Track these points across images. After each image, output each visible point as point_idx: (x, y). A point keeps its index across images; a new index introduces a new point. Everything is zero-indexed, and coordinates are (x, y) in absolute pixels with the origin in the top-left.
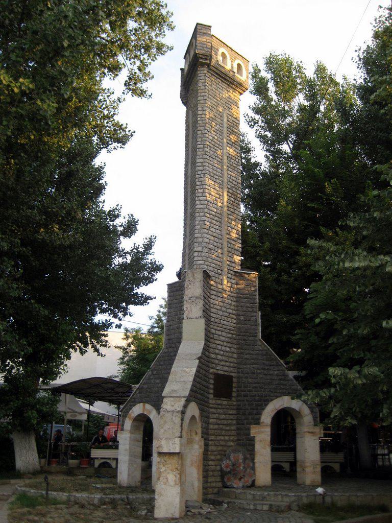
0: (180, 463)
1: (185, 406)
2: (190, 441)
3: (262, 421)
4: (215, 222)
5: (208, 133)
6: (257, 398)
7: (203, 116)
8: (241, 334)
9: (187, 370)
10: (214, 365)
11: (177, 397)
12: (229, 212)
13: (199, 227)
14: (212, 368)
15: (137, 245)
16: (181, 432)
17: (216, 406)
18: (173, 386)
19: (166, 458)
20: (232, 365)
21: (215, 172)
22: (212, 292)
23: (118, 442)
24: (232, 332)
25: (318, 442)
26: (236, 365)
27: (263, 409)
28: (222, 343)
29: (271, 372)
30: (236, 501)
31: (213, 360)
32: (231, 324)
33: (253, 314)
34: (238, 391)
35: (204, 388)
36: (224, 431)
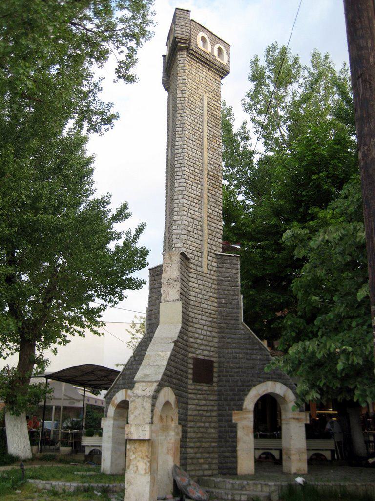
0: (150, 451)
1: (157, 391)
2: (165, 429)
3: (244, 407)
5: (187, 115)
6: (239, 383)
7: (182, 99)
8: (223, 317)
9: (161, 354)
10: (193, 350)
11: (149, 381)
12: (210, 195)
13: (177, 209)
14: (191, 353)
16: (152, 418)
17: (196, 392)
18: (146, 370)
19: (137, 445)
20: (212, 349)
21: (194, 154)
22: (191, 275)
23: (102, 429)
24: (212, 315)
25: (304, 429)
26: (217, 349)
27: (246, 395)
28: (202, 327)
29: (254, 357)
30: (214, 490)
31: (192, 344)
32: (212, 307)
34: (219, 376)
35: (182, 373)
36: (204, 418)
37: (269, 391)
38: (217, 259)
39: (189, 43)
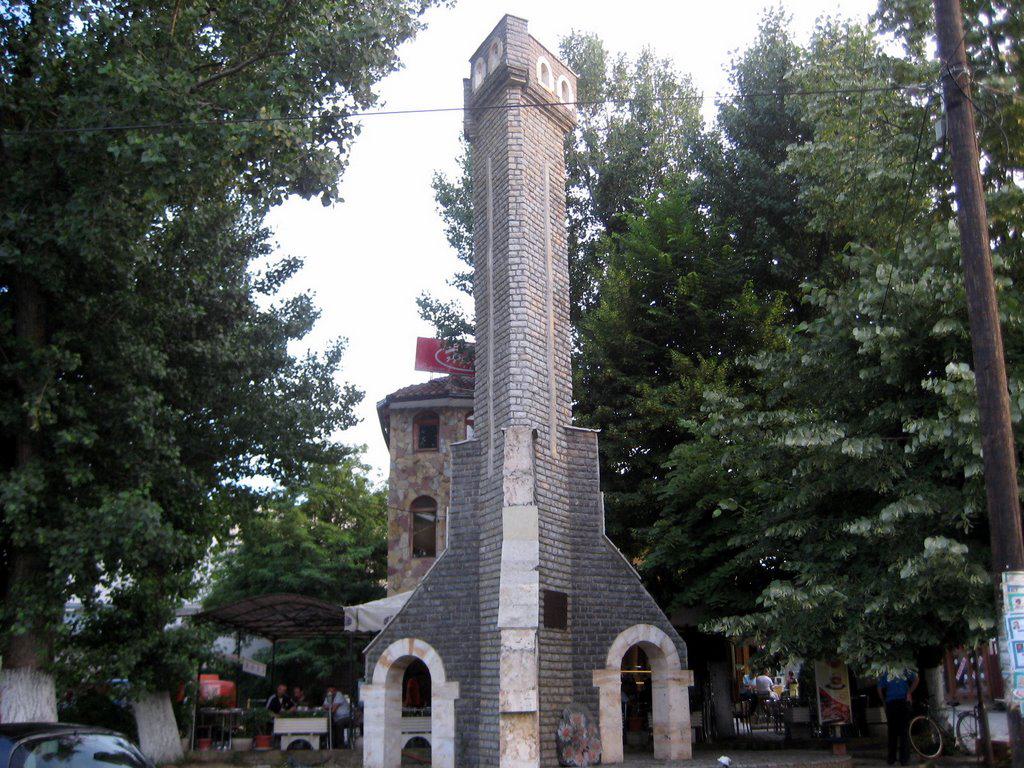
3: (608, 663)
4: (538, 348)
6: (601, 628)
7: (517, 172)
11: (522, 628)
13: (516, 357)
15: (312, 353)
19: (515, 720)
20: (565, 576)
27: (610, 645)
29: (620, 587)
33: (593, 496)
37: (641, 639)
38: (566, 435)
39: (527, 79)
